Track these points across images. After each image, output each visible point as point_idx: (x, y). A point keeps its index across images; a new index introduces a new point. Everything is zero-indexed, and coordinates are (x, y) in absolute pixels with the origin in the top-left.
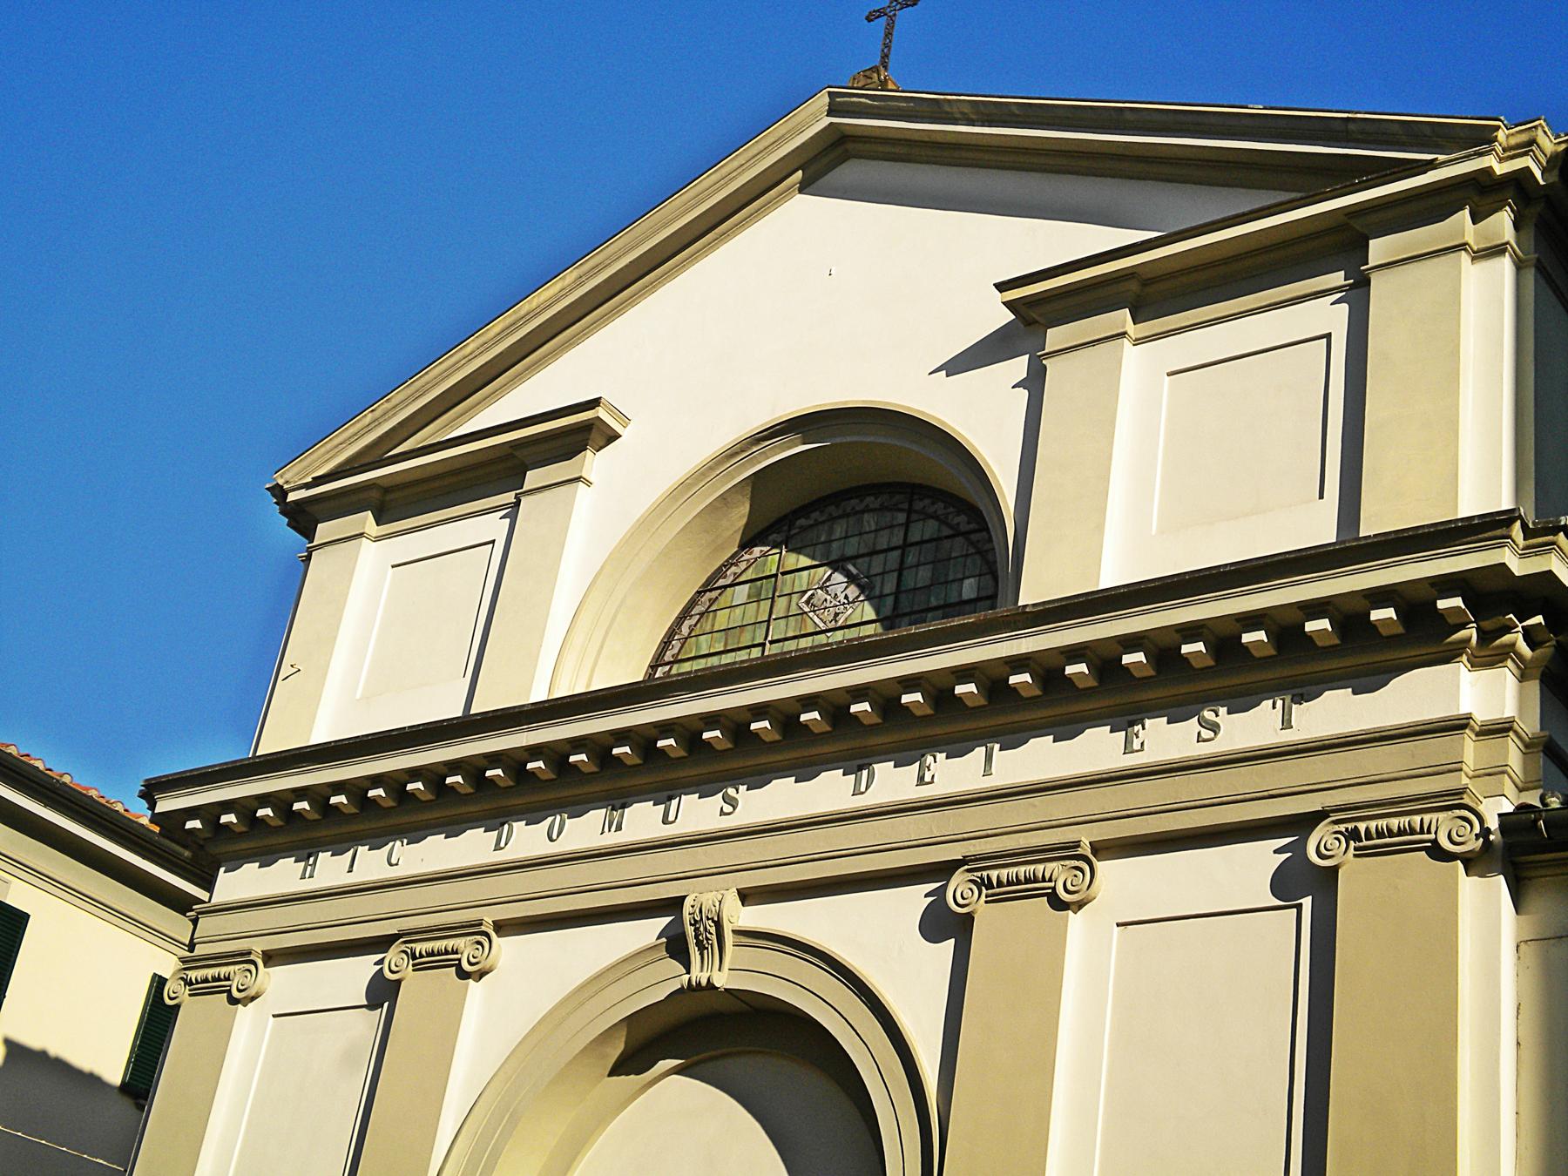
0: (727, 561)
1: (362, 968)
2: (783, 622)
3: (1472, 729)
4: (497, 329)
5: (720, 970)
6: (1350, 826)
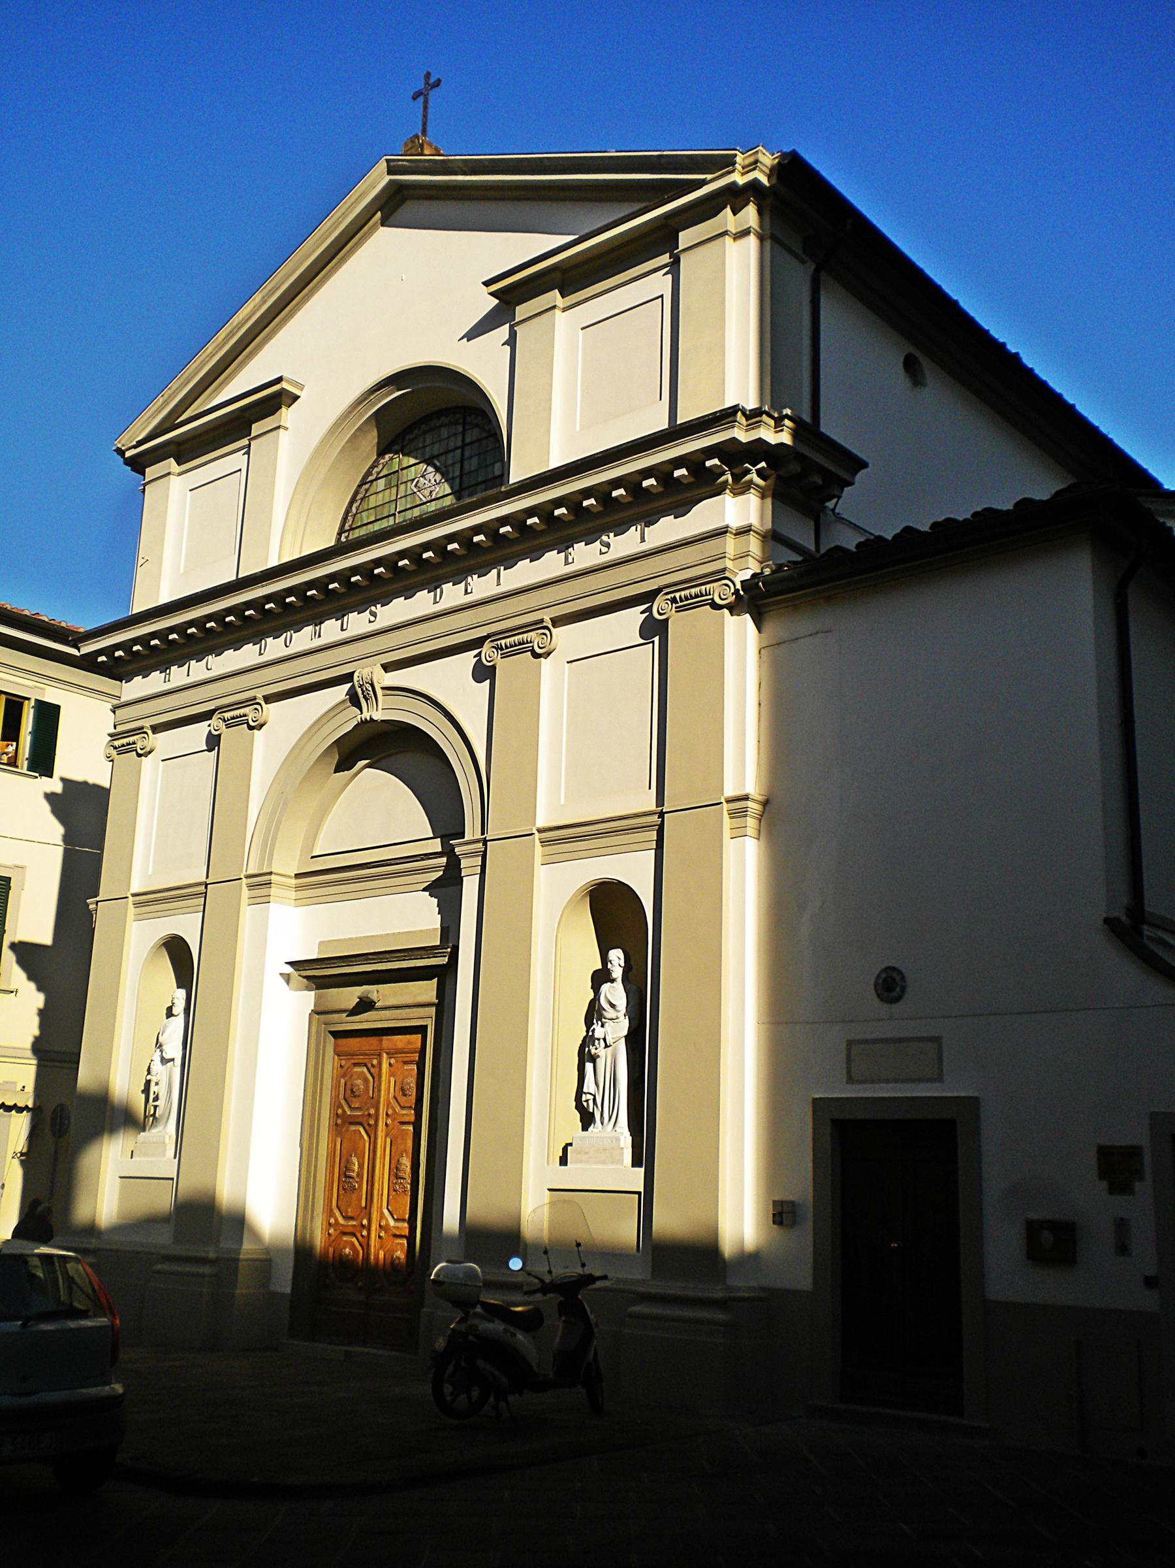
0: (372, 464)
1: (201, 730)
2: (404, 499)
3: (731, 533)
4: (223, 336)
5: (377, 710)
6: (672, 595)
